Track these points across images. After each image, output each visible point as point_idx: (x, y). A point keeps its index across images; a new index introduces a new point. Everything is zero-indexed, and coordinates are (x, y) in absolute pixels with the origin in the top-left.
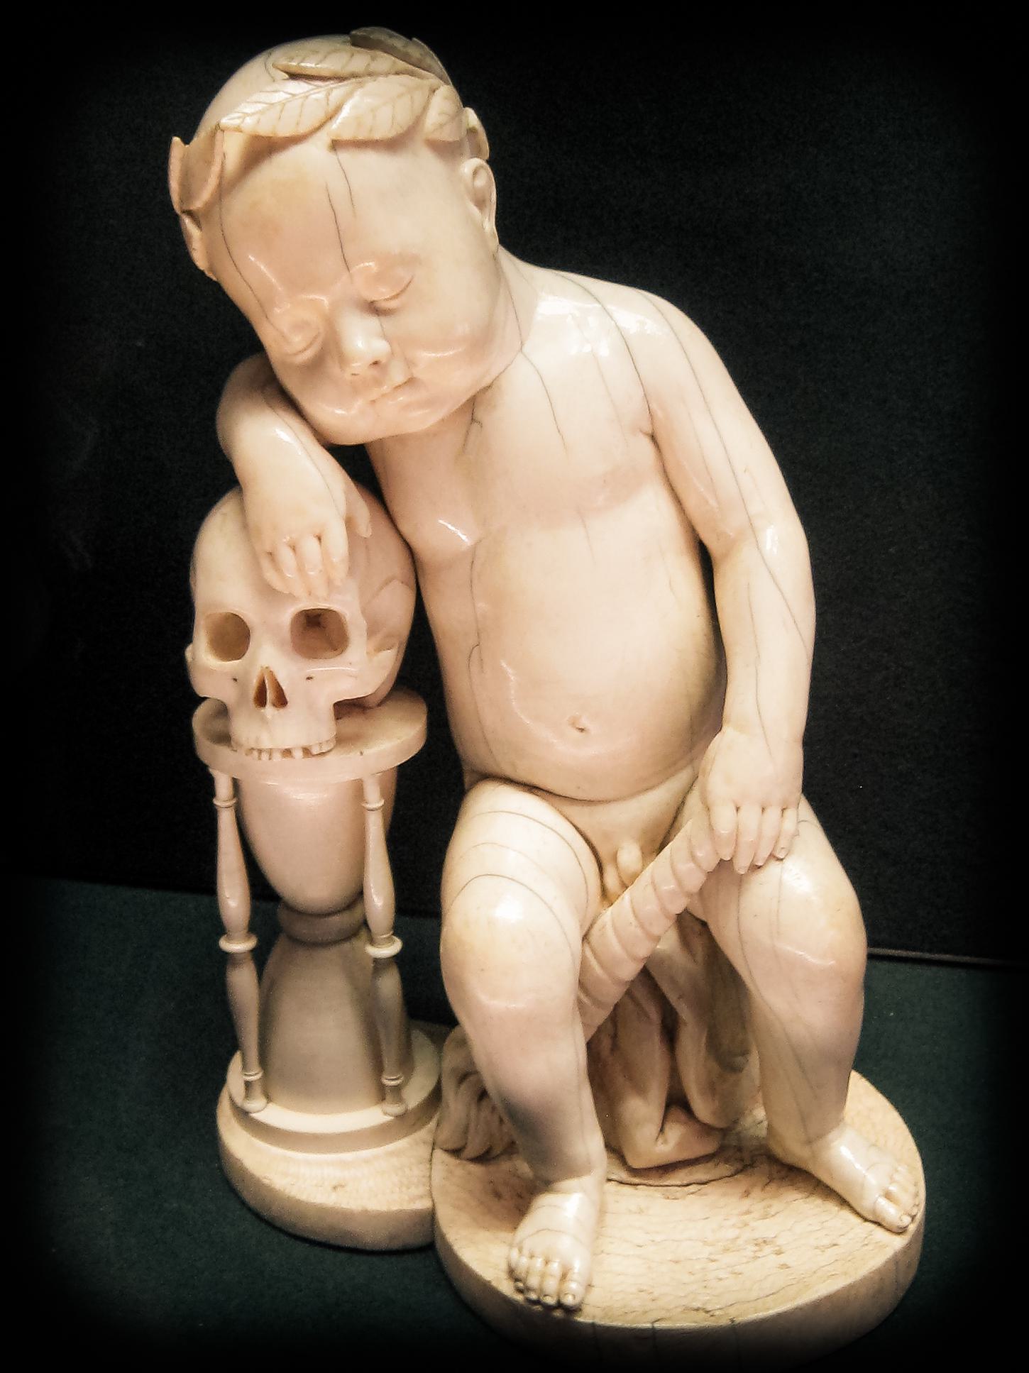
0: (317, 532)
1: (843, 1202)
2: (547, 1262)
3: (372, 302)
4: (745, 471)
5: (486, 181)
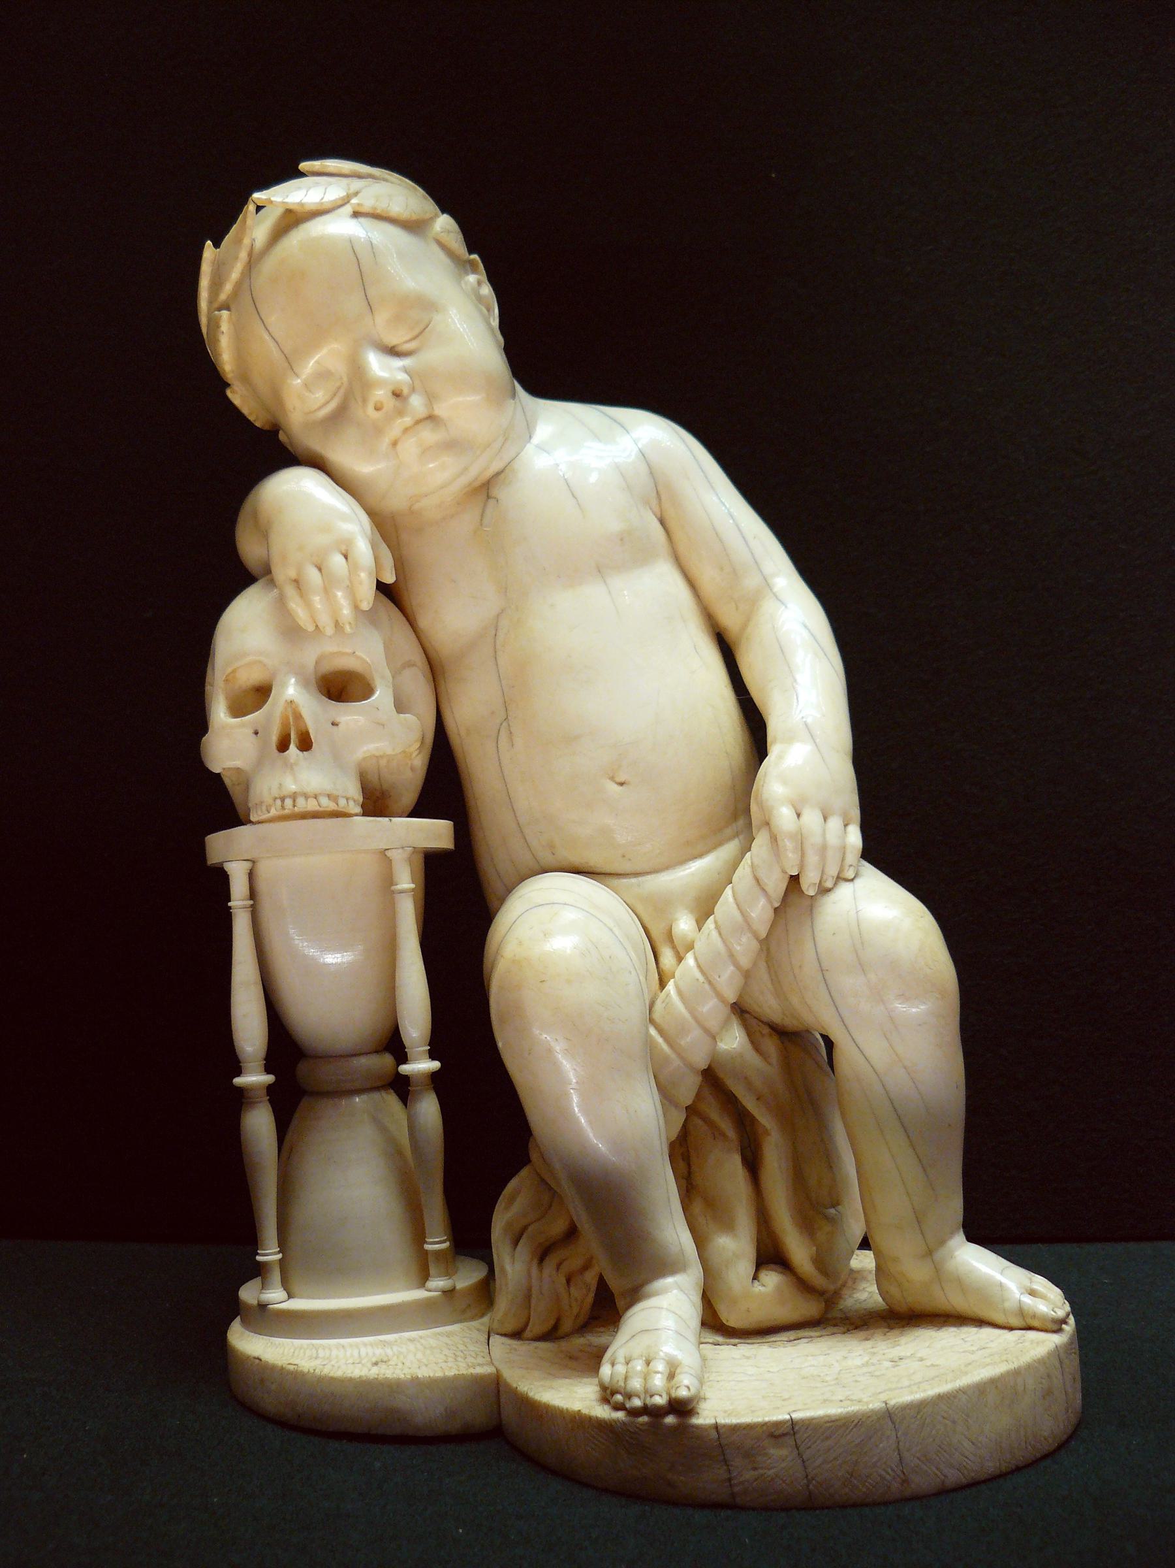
0: (343, 548)
1: (980, 1322)
2: (648, 1363)
3: (393, 347)
4: (755, 538)
5: (487, 290)
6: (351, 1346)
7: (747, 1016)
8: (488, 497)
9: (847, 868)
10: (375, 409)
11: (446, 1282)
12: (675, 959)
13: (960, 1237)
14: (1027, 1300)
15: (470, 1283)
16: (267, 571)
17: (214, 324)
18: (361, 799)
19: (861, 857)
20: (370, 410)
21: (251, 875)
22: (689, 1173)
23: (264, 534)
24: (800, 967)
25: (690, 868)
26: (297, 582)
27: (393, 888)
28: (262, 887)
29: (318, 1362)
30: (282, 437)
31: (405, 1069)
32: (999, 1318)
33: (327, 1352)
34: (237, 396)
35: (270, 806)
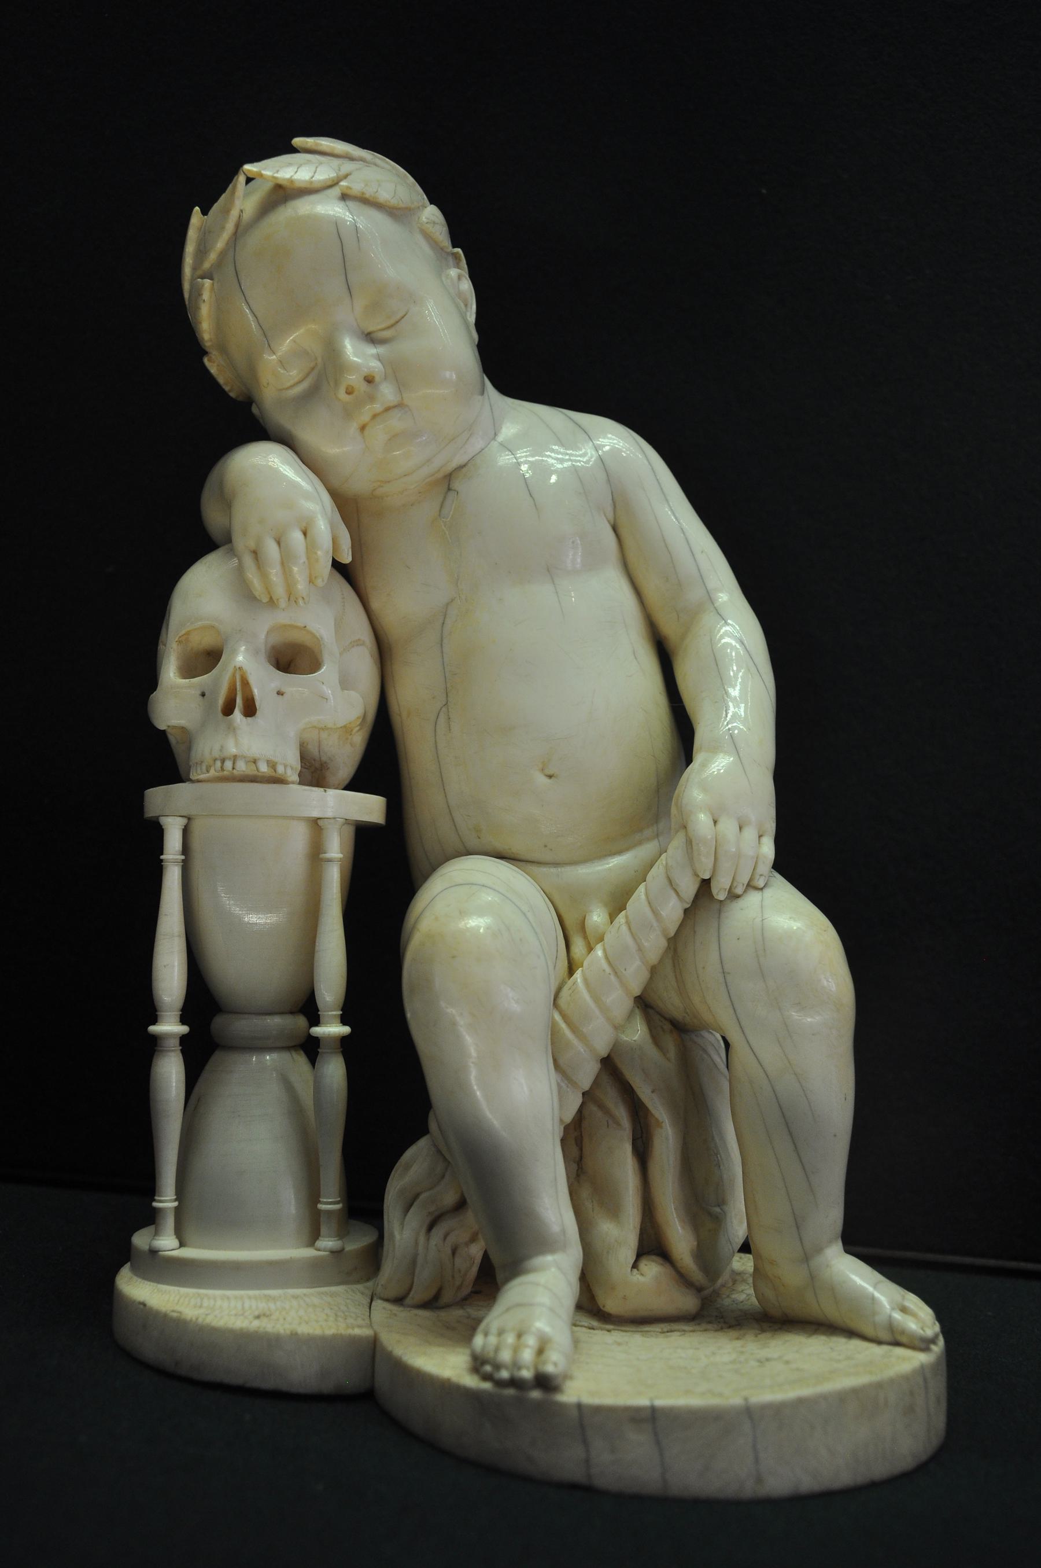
1: (851, 1333)
2: (519, 1336)
4: (702, 552)
5: (467, 286)
6: (236, 1298)
7: (651, 1011)
8: (449, 489)
9: (757, 877)
10: (346, 392)
11: (334, 1242)
12: (586, 950)
13: (837, 1247)
14: (897, 1316)
15: (362, 1245)
16: (228, 540)
17: (197, 292)
18: (299, 768)
19: (773, 868)
20: (342, 395)
21: (186, 832)
22: (581, 1158)
23: (227, 503)
24: (704, 968)
25: (608, 864)
26: (255, 554)
27: (322, 856)
28: (196, 843)
29: (202, 1311)
30: (255, 410)
31: (317, 1031)
32: (869, 1331)
33: (212, 1302)
34: (214, 365)
35: (210, 767)
